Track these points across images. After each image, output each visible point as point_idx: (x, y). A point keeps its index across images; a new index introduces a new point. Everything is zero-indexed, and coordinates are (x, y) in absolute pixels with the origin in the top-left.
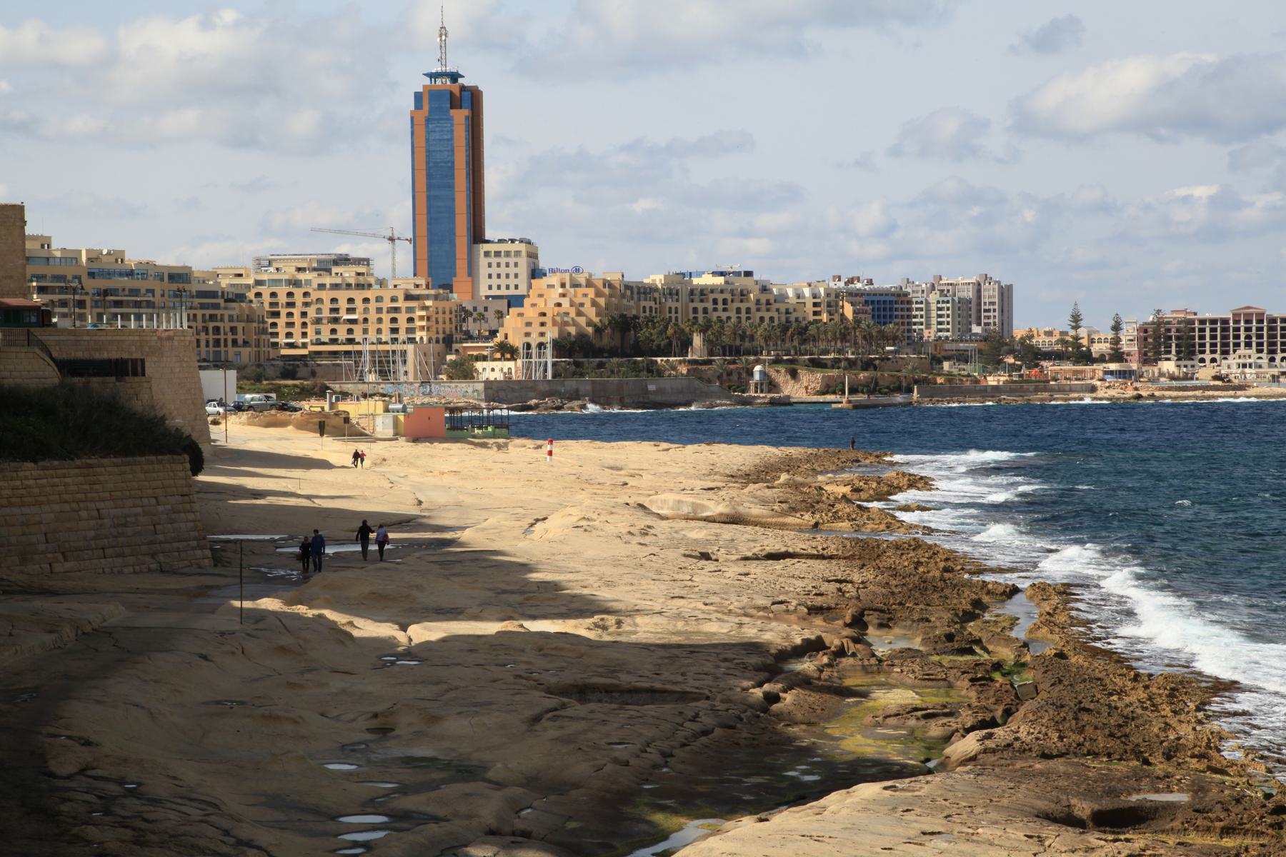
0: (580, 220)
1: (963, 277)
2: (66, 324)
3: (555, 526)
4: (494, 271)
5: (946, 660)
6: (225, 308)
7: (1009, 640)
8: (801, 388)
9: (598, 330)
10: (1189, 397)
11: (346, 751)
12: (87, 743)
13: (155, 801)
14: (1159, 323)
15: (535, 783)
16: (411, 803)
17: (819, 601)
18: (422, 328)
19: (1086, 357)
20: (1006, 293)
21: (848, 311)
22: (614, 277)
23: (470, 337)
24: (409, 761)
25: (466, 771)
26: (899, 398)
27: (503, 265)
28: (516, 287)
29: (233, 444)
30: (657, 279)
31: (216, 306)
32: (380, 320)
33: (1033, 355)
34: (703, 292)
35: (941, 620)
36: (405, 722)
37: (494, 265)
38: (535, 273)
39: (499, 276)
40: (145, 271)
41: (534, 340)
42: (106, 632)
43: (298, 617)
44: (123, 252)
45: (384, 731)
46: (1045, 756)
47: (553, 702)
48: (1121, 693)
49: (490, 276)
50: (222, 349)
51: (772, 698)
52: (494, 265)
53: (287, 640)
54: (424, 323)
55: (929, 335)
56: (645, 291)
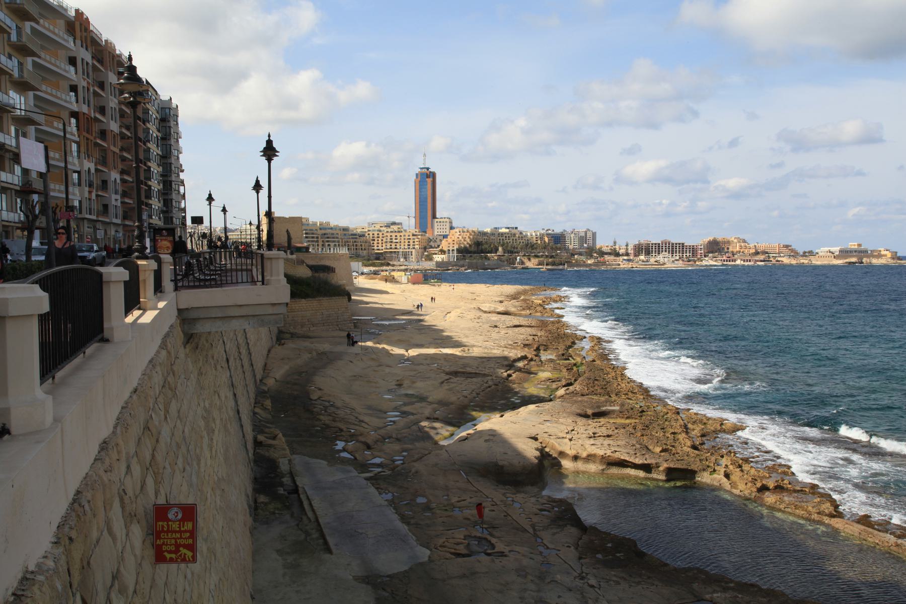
0: (466, 213)
1: (581, 230)
2: (313, 252)
3: (453, 316)
5: (561, 362)
7: (579, 355)
8: (531, 264)
9: (470, 246)
10: (649, 267)
11: (390, 391)
12: (320, 389)
13: (338, 408)
14: (639, 245)
15: (442, 403)
16: (406, 409)
17: (527, 342)
19: (617, 255)
20: (594, 234)
21: (546, 239)
22: (475, 229)
23: (431, 247)
24: (407, 395)
25: (422, 399)
26: (561, 267)
29: (361, 286)
30: (488, 230)
33: (602, 253)
34: (502, 234)
35: (561, 348)
36: (406, 383)
38: (452, 228)
40: (336, 228)
41: (451, 249)
42: (324, 353)
43: (377, 348)
45: (400, 385)
46: (583, 395)
47: (448, 377)
48: (607, 374)
51: (510, 376)
53: (374, 356)
55: (571, 247)
56: (485, 234)
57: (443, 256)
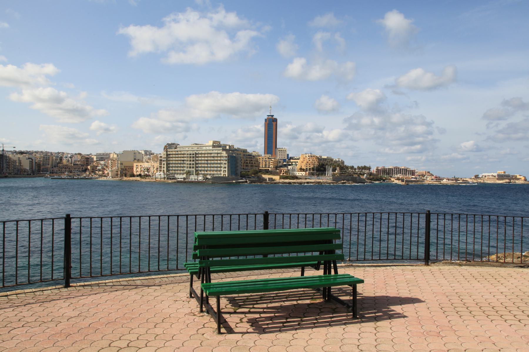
41: (308, 168)
57: (302, 173)
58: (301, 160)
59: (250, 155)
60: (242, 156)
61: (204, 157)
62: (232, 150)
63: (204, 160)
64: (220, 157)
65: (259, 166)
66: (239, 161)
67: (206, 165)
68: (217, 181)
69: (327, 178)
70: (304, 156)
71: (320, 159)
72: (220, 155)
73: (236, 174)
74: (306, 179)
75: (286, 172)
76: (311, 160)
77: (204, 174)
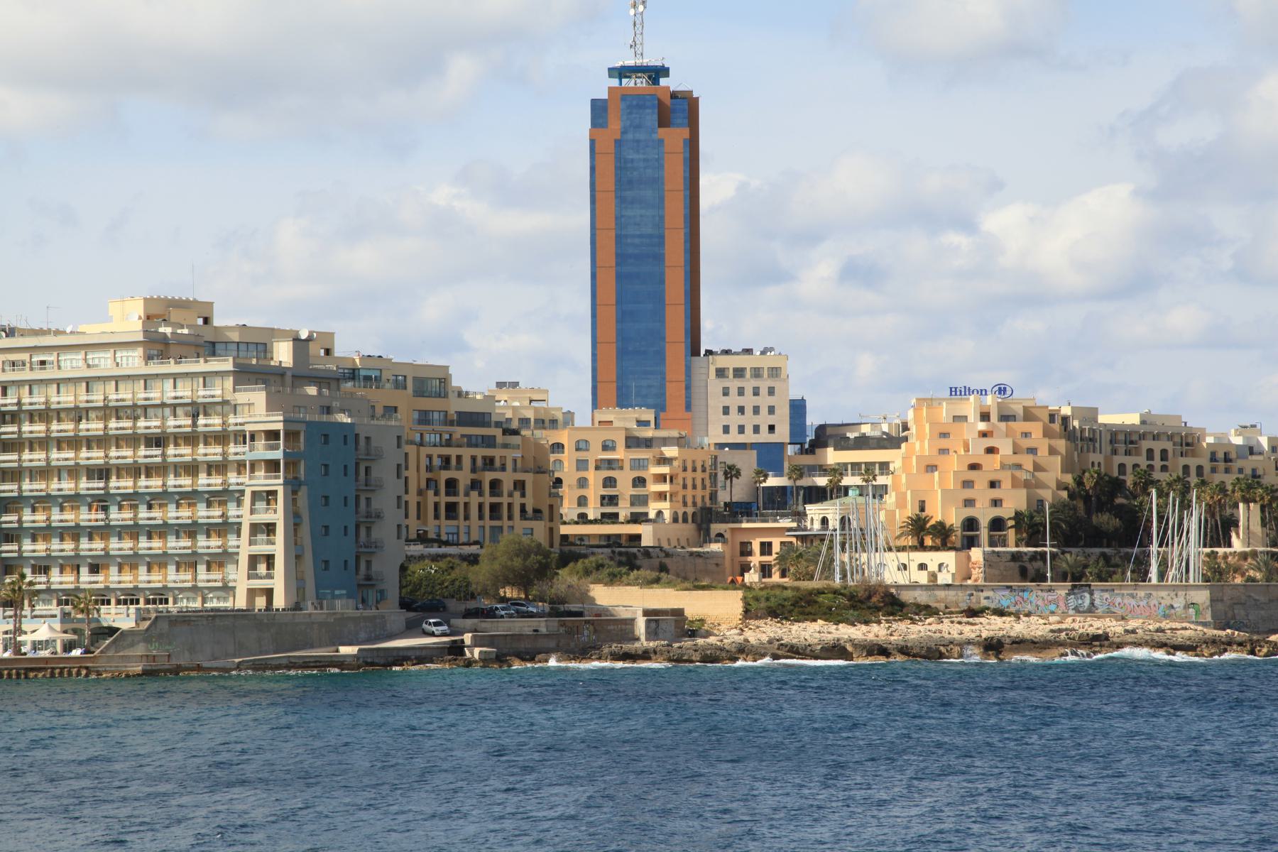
4: (733, 401)
6: (505, 446)
18: (661, 496)
27: (749, 391)
28: (772, 428)
31: (489, 442)
32: (582, 483)
37: (733, 391)
39: (756, 410)
41: (985, 516)
44: (331, 335)
49: (726, 411)
50: (505, 523)
52: (733, 391)
54: (665, 487)
57: (932, 559)
58: (920, 445)
59: (477, 419)
60: (404, 419)
61: (74, 443)
62: (321, 380)
63: (73, 472)
64: (221, 438)
65: (550, 513)
66: (384, 471)
67: (86, 517)
68: (187, 653)
69: (1155, 611)
70: (944, 413)
71: (1079, 436)
72: (212, 423)
73: (365, 588)
74: (973, 613)
75: (789, 557)
76: (1005, 448)
77: (68, 597)
